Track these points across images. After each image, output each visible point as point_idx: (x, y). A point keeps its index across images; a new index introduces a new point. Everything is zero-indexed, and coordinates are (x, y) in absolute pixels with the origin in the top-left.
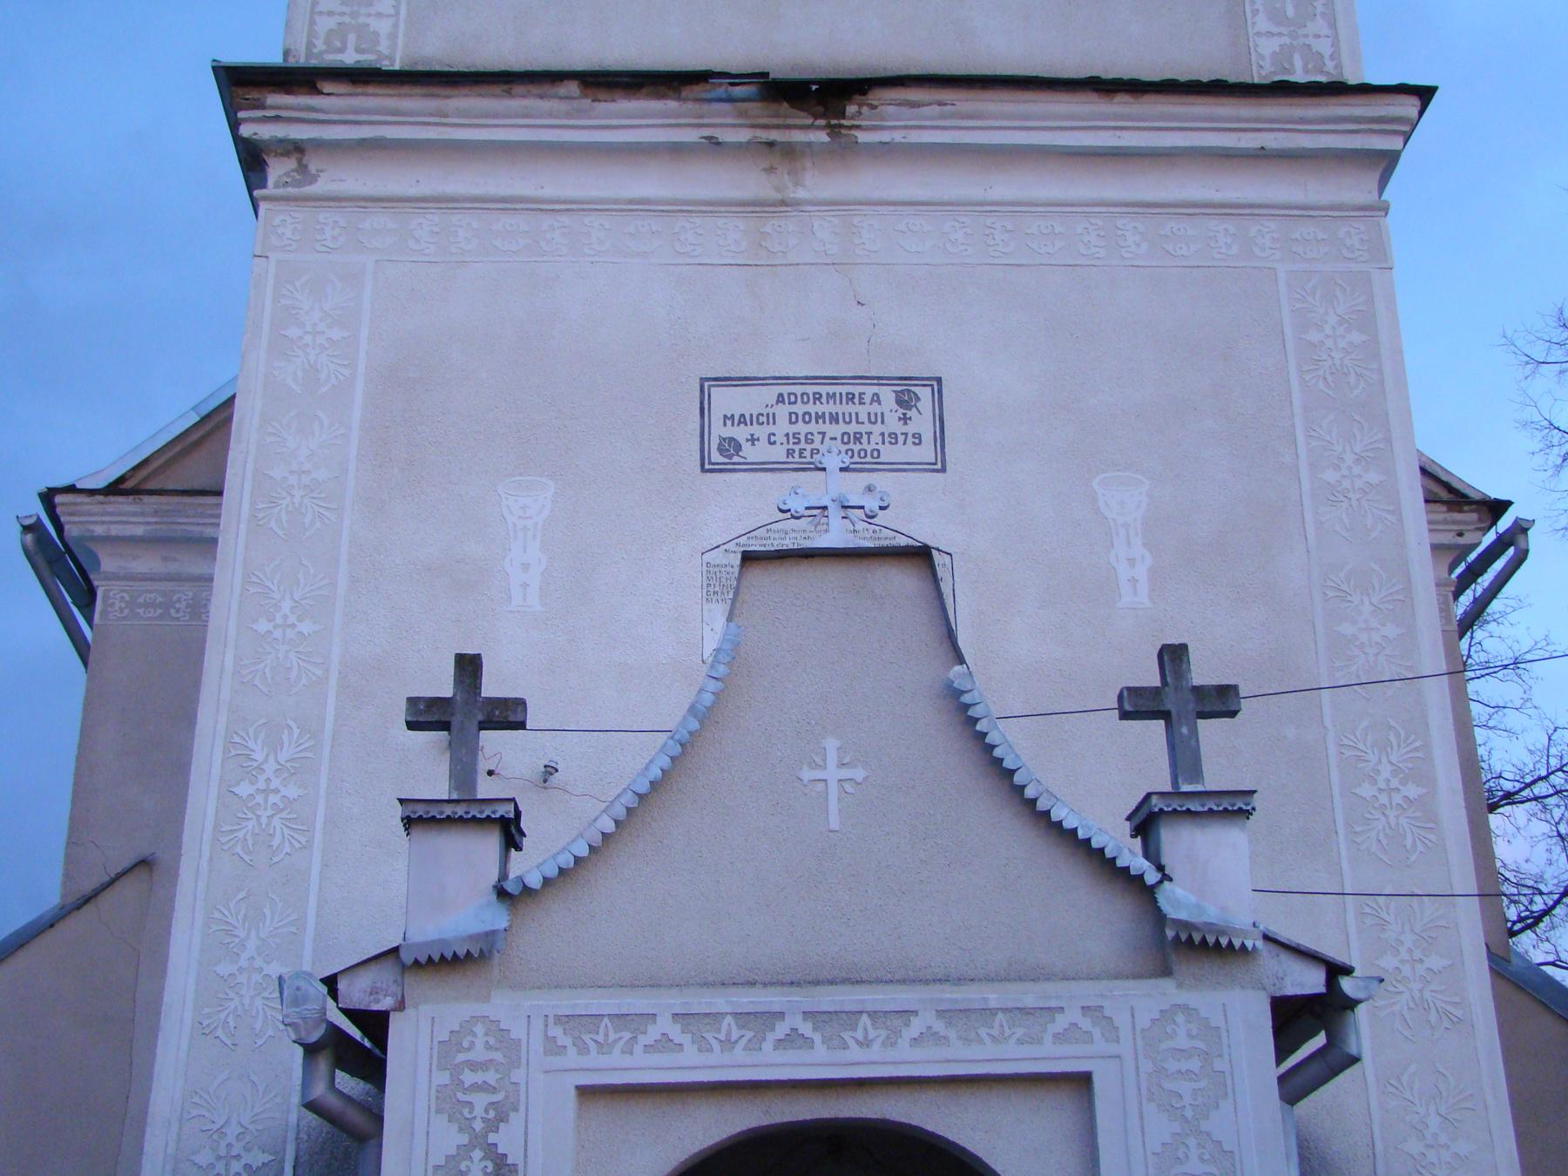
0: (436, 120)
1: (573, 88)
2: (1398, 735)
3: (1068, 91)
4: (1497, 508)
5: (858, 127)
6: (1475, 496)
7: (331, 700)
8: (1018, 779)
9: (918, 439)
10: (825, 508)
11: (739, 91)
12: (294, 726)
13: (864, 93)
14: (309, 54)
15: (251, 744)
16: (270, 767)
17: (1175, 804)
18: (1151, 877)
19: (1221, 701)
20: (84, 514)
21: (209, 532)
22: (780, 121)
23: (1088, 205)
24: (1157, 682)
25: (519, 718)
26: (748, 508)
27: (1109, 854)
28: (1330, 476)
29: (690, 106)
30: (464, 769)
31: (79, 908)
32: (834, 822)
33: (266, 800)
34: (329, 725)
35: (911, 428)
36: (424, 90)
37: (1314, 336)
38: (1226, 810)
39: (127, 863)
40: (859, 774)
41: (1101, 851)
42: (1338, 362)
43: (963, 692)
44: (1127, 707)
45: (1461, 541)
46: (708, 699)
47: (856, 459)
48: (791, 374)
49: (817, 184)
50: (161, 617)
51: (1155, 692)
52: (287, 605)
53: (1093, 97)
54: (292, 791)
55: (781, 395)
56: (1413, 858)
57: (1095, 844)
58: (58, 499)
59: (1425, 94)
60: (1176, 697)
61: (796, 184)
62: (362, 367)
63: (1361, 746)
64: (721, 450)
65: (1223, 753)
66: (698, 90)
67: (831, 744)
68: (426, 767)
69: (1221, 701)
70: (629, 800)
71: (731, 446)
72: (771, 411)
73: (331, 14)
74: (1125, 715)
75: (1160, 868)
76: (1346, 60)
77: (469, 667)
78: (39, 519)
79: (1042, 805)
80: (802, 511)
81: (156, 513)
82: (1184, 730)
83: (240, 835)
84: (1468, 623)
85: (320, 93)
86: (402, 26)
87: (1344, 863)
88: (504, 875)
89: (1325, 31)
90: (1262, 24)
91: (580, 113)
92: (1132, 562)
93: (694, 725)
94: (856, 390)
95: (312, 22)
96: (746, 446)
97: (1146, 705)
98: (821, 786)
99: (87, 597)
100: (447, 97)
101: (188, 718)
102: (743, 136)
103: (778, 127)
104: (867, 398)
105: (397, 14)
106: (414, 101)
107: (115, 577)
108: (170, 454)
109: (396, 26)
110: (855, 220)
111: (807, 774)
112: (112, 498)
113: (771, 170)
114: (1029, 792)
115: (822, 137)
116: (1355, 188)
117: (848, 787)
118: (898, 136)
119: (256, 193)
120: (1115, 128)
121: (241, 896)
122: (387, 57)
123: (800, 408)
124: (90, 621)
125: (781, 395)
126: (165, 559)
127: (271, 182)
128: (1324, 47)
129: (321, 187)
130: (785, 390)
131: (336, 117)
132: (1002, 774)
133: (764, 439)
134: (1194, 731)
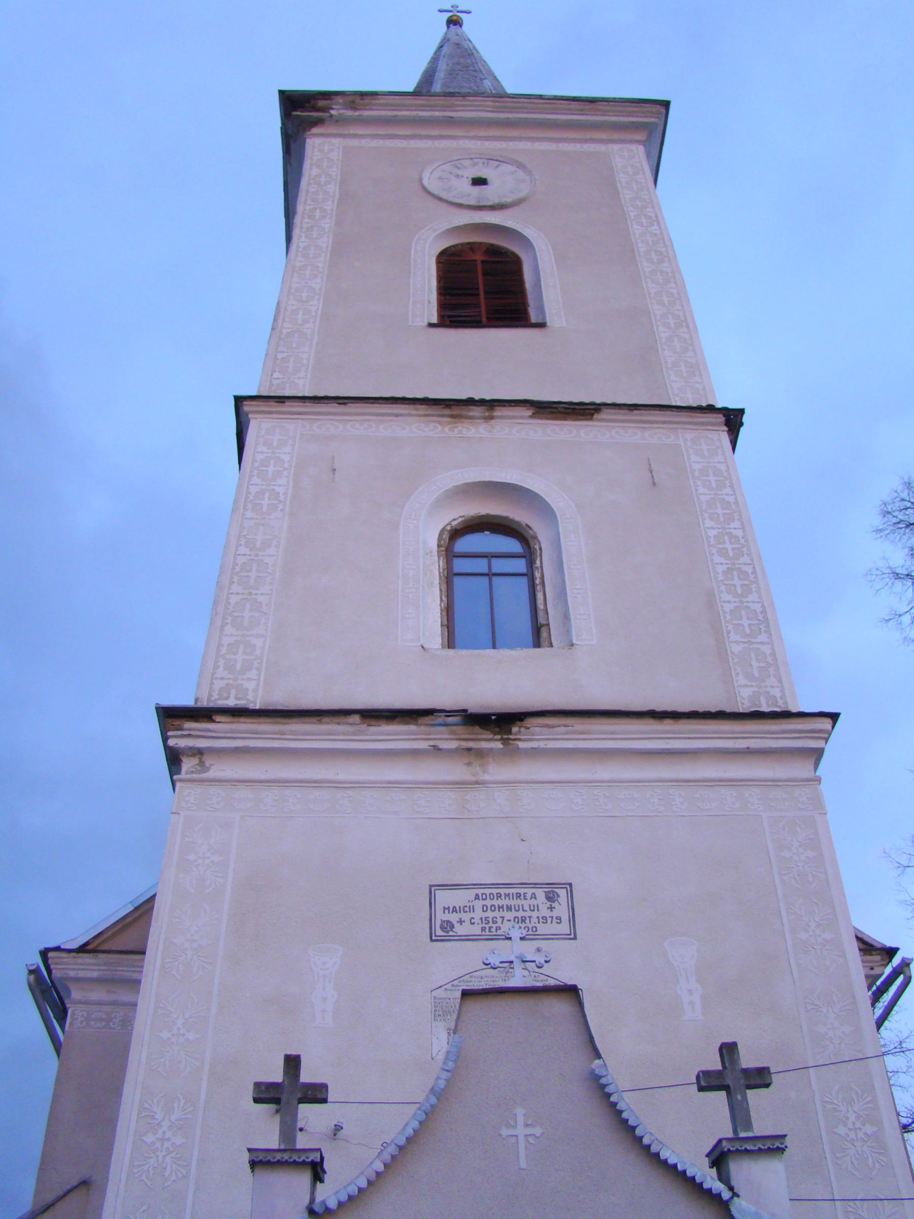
1: (356, 718)
3: (638, 718)
4: (891, 952)
5: (519, 739)
6: (879, 946)
8: (638, 1132)
9: (559, 919)
10: (511, 962)
11: (450, 720)
12: (181, 1098)
13: (522, 720)
14: (209, 700)
16: (165, 1125)
17: (737, 1145)
18: (726, 1195)
19: (760, 1078)
21: (135, 976)
22: (472, 736)
23: (649, 782)
25: (324, 1097)
26: (465, 963)
28: (803, 936)
29: (423, 728)
30: (289, 1130)
31: (43, 1212)
32: (523, 1164)
33: (162, 1145)
35: (555, 913)
37: (786, 854)
39: (75, 1182)
40: (538, 1131)
41: (693, 1178)
43: (600, 1077)
44: (703, 1083)
45: (872, 972)
46: (442, 1083)
47: (530, 932)
49: (497, 771)
50: (104, 1027)
51: (719, 1074)
53: (651, 721)
54: (179, 1140)
55: (477, 895)
56: (874, 1173)
57: (689, 1173)
58: (50, 954)
59: (834, 717)
60: (732, 1077)
61: (484, 772)
63: (836, 1102)
64: (442, 928)
65: (765, 1111)
66: (428, 719)
67: (520, 1112)
69: (760, 1078)
71: (447, 926)
72: (471, 904)
73: (222, 679)
74: (701, 1089)
75: (731, 1188)
76: (789, 700)
77: (292, 1063)
78: (38, 967)
79: (654, 1149)
80: (498, 964)
81: (105, 964)
82: (739, 1097)
83: (146, 1167)
84: (880, 1022)
85: (214, 721)
86: (261, 683)
87: (832, 1176)
88: (312, 1200)
89: (776, 684)
90: (741, 680)
91: (359, 733)
92: (690, 992)
94: (522, 891)
95: (212, 684)
96: (457, 925)
97: (716, 1082)
98: (513, 1140)
99: (62, 1014)
101: (118, 1091)
103: (473, 740)
104: (529, 896)
105: (259, 679)
107: (80, 1002)
108: (115, 929)
109: (258, 685)
111: (505, 1132)
112: (80, 955)
113: (469, 764)
114: (646, 1141)
115: (499, 745)
116: (800, 769)
117: (531, 1140)
118: (542, 744)
119: (175, 777)
121: (144, 1208)
122: (252, 702)
123: (488, 903)
124: (63, 1028)
125: (477, 895)
126: (108, 992)
128: (777, 693)
129: (212, 774)
130: (480, 892)
132: (628, 1129)
134: (745, 1097)
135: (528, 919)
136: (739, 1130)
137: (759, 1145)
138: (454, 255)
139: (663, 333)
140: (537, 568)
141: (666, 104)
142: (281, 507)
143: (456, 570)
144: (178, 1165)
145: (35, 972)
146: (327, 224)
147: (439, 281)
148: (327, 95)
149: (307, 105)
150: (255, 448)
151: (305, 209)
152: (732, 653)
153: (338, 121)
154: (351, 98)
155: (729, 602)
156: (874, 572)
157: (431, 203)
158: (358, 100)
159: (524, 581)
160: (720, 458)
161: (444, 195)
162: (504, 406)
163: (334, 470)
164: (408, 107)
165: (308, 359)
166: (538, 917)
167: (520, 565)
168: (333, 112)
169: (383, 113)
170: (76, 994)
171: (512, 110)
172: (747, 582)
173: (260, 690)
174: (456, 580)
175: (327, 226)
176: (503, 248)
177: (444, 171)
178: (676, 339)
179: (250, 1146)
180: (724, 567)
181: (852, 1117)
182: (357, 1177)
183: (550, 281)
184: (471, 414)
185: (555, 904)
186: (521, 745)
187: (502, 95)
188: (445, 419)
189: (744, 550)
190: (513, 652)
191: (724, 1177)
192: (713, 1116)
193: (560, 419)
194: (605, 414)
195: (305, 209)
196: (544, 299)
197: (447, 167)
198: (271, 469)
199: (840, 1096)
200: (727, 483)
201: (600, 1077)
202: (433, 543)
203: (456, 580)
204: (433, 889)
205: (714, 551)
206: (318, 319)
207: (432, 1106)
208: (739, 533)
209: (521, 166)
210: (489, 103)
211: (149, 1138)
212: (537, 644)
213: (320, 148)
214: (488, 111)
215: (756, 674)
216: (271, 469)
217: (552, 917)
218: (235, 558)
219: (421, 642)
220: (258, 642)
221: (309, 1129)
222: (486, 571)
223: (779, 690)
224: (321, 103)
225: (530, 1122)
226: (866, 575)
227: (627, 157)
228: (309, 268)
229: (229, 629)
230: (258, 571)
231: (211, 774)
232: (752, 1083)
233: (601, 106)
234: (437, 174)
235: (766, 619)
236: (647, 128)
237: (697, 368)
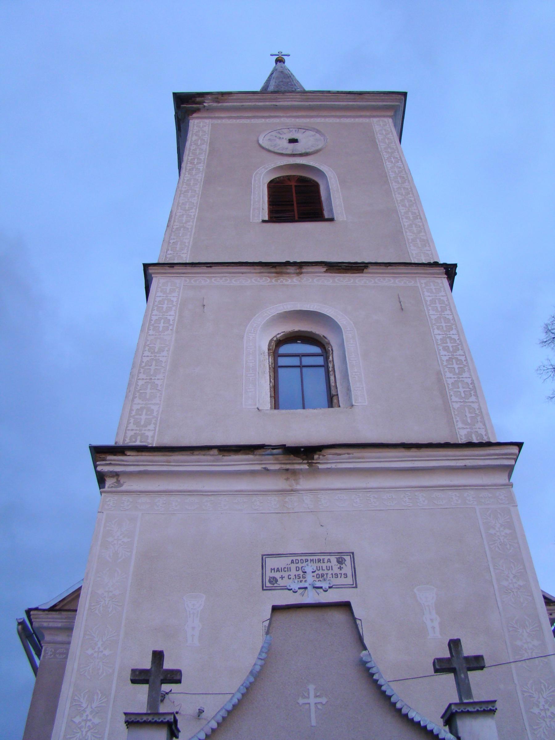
0: (167, 464)
1: (215, 451)
2: (545, 686)
5: (319, 463)
7: (115, 682)
8: (393, 700)
9: (346, 576)
11: (275, 451)
12: (99, 693)
15: (82, 700)
16: (88, 710)
17: (462, 708)
20: (40, 618)
22: (290, 462)
24: (448, 655)
25: (178, 678)
27: (435, 732)
28: (505, 583)
29: (257, 457)
34: (113, 692)
35: (343, 571)
36: (163, 454)
37: (492, 531)
38: (484, 710)
40: (324, 700)
42: (502, 540)
43: (367, 662)
44: (438, 667)
46: (258, 668)
48: (297, 552)
49: (304, 483)
51: (448, 660)
52: (100, 644)
53: (403, 450)
54: (97, 720)
55: (292, 560)
58: (32, 613)
59: (519, 445)
60: (456, 663)
61: (297, 484)
62: (134, 552)
63: (531, 691)
64: (270, 582)
65: (481, 685)
67: (311, 687)
68: (139, 698)
69: (477, 663)
70: (223, 713)
71: (273, 580)
72: (289, 566)
73: (132, 430)
76: (490, 435)
77: (158, 656)
78: (24, 620)
79: (404, 711)
82: (463, 676)
86: (157, 433)
90: (460, 425)
91: (217, 461)
92: (432, 620)
93: (252, 679)
94: (321, 558)
95: (126, 433)
96: (280, 580)
100: (171, 456)
102: (277, 467)
103: (290, 464)
104: (326, 561)
105: (155, 430)
106: (159, 457)
108: (72, 597)
109: (154, 433)
110: (319, 496)
111: (301, 701)
112: (51, 613)
113: (287, 479)
114: (398, 705)
115: (306, 467)
116: (500, 479)
117: (319, 706)
118: (333, 466)
120: (412, 460)
122: (150, 444)
124: (39, 655)
127: (107, 486)
128: (483, 432)
129: (124, 488)
130: (294, 558)
131: (131, 463)
132: (385, 698)
133: (286, 578)
134: (467, 677)
135: (325, 575)
136: (463, 698)
137: (478, 708)
138: (278, 182)
139: (405, 223)
140: (330, 361)
141: (405, 94)
142: (170, 328)
143: (280, 364)
144: (96, 737)
145: (22, 623)
146: (201, 167)
147: (269, 198)
148: (202, 95)
149: (190, 101)
150: (156, 294)
151: (188, 159)
152: (453, 408)
153: (208, 109)
154: (216, 96)
155: (451, 378)
156: (542, 368)
157: (265, 153)
158: (220, 97)
159: (322, 371)
160: (443, 293)
161: (271, 149)
162: (308, 266)
163: (204, 306)
164: (250, 100)
165: (189, 243)
166: (332, 574)
167: (320, 361)
168: (205, 104)
169: (235, 104)
170: (48, 638)
171: (313, 100)
172: (462, 366)
173: (156, 437)
174: (280, 370)
175: (201, 168)
176: (308, 178)
177: (272, 135)
178: (414, 226)
179: (126, 712)
180: (447, 358)
181: (542, 701)
182: (199, 732)
183: (336, 194)
184: (288, 271)
185: (343, 566)
186: (320, 466)
187: (305, 92)
188: (274, 275)
189: (459, 347)
190: (315, 411)
191: (453, 731)
192: (446, 689)
193: (343, 273)
194: (371, 269)
195: (188, 159)
196: (333, 205)
197: (274, 133)
198: (165, 306)
199: (533, 687)
200: (448, 308)
201: (367, 662)
202: (265, 348)
203: (280, 370)
204: (264, 557)
205: (441, 348)
206: (195, 220)
207: (250, 683)
208: (456, 337)
209: (318, 131)
210: (298, 96)
211: (77, 719)
212: (331, 404)
213: (198, 126)
214: (298, 101)
215: (469, 421)
216: (165, 306)
217: (341, 574)
218: (142, 358)
219: (257, 406)
220: (155, 408)
221: (182, 713)
222: (299, 364)
223: (484, 430)
224: (198, 99)
225: (318, 694)
226: (537, 370)
227: (382, 126)
228: (190, 191)
229: (137, 400)
230: (156, 365)
231: (124, 488)
232: (471, 666)
233: (366, 96)
234: (268, 137)
235: (474, 387)
236: (394, 109)
237: (427, 242)
